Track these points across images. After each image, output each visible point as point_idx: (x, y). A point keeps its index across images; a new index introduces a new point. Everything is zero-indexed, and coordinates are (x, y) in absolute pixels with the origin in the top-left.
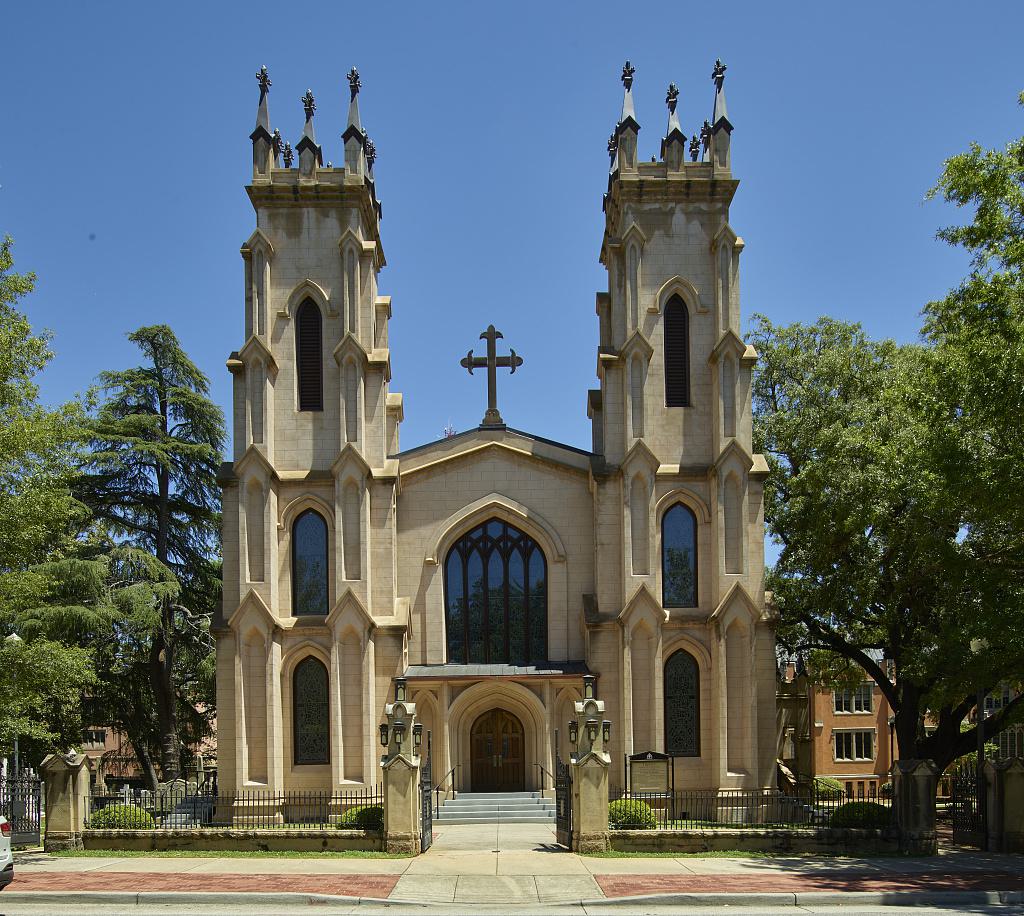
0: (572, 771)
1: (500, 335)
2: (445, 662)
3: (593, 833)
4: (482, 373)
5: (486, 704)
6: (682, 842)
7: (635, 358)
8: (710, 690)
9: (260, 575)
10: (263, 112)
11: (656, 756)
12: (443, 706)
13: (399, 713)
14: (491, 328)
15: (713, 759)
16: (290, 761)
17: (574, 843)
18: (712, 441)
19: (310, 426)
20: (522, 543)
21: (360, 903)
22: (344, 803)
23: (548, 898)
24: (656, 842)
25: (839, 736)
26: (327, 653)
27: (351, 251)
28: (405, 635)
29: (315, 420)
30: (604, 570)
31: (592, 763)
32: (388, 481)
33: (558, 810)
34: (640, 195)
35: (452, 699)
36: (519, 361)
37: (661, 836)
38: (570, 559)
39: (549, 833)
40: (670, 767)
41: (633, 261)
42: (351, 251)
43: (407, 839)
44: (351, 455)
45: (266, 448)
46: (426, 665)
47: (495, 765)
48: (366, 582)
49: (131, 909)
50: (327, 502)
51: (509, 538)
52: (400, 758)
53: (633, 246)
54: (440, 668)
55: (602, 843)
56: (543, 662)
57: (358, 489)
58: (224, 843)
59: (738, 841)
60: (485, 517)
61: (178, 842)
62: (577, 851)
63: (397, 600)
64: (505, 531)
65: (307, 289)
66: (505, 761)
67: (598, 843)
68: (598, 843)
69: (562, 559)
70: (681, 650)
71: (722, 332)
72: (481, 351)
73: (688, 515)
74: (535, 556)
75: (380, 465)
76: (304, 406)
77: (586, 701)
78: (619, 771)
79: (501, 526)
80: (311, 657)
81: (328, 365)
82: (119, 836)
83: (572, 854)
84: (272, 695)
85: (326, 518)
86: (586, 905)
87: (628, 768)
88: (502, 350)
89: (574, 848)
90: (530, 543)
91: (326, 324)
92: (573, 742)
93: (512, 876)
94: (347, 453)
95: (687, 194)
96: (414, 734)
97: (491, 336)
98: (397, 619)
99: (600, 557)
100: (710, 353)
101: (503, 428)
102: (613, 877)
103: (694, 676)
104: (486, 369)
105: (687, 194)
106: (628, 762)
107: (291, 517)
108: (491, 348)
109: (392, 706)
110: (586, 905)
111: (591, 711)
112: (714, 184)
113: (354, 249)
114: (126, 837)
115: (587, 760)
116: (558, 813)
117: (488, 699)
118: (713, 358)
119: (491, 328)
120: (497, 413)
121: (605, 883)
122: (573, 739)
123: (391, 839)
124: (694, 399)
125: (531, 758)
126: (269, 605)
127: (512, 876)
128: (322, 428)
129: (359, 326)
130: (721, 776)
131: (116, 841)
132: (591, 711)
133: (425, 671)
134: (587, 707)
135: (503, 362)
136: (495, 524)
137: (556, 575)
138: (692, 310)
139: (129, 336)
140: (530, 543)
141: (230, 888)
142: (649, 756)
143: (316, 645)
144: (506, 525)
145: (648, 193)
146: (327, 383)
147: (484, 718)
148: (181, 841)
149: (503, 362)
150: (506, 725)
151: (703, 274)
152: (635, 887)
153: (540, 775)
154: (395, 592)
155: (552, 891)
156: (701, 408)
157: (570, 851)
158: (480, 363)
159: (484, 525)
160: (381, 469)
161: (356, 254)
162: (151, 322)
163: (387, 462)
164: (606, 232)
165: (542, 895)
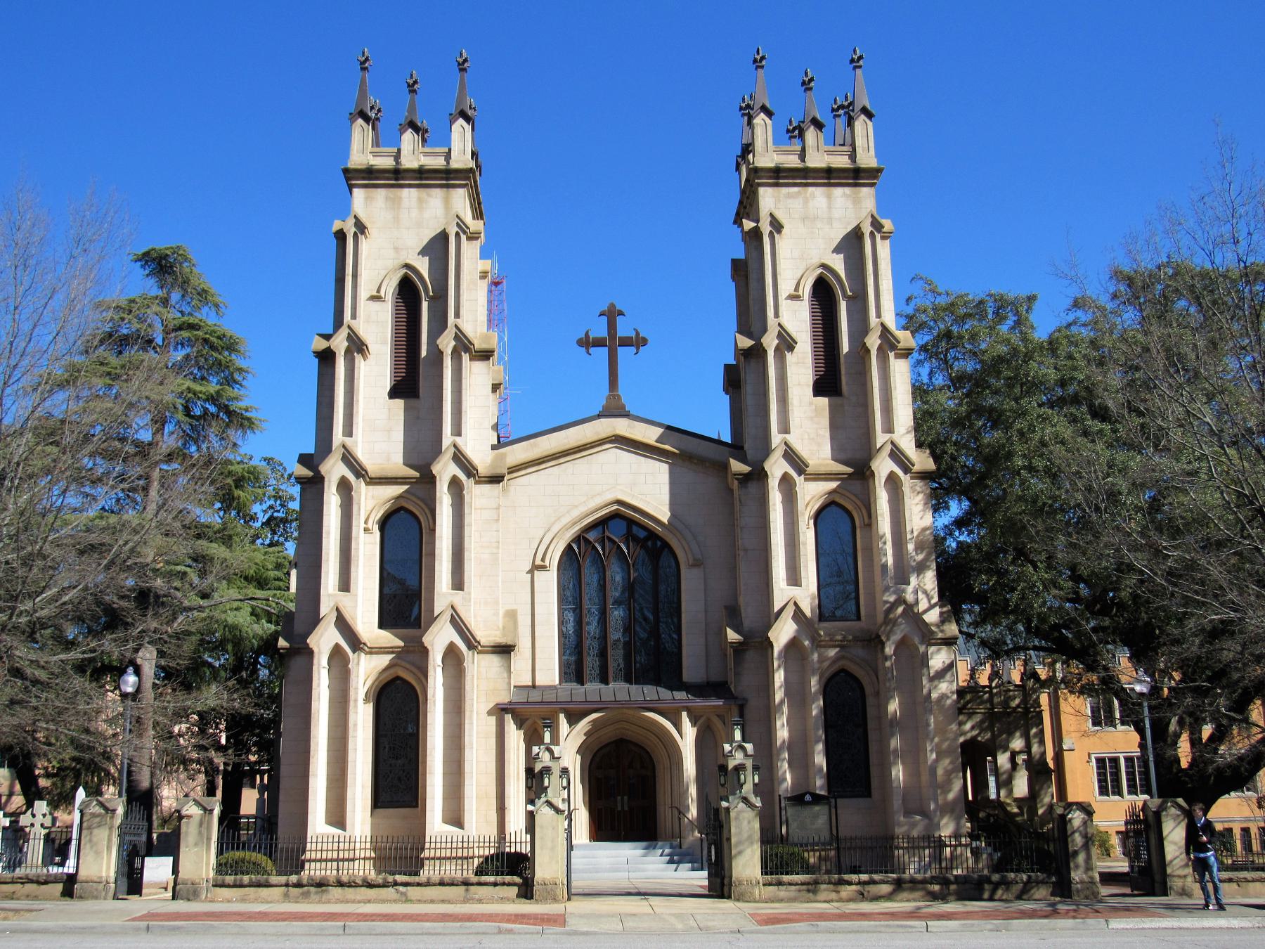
1: (621, 313)
4: (603, 352)
10: (363, 82)
11: (817, 799)
14: (612, 306)
17: (726, 889)
20: (650, 543)
23: (707, 928)
25: (1101, 762)
36: (644, 342)
40: (833, 810)
45: (356, 442)
47: (619, 808)
50: (422, 500)
56: (676, 683)
69: (697, 564)
72: (600, 329)
73: (845, 515)
74: (665, 559)
78: (774, 816)
79: (623, 524)
80: (398, 678)
84: (355, 725)
85: (420, 517)
88: (624, 330)
89: (726, 894)
90: (659, 543)
97: (612, 315)
104: (606, 349)
106: (783, 805)
108: (612, 326)
119: (612, 306)
121: (758, 918)
124: (845, 388)
128: (418, 418)
135: (626, 342)
136: (617, 521)
137: (690, 581)
139: (131, 257)
140: (659, 543)
142: (808, 798)
143: (408, 666)
149: (626, 342)
155: (710, 924)
158: (599, 343)
162: (161, 243)
164: (741, 202)
165: (701, 925)
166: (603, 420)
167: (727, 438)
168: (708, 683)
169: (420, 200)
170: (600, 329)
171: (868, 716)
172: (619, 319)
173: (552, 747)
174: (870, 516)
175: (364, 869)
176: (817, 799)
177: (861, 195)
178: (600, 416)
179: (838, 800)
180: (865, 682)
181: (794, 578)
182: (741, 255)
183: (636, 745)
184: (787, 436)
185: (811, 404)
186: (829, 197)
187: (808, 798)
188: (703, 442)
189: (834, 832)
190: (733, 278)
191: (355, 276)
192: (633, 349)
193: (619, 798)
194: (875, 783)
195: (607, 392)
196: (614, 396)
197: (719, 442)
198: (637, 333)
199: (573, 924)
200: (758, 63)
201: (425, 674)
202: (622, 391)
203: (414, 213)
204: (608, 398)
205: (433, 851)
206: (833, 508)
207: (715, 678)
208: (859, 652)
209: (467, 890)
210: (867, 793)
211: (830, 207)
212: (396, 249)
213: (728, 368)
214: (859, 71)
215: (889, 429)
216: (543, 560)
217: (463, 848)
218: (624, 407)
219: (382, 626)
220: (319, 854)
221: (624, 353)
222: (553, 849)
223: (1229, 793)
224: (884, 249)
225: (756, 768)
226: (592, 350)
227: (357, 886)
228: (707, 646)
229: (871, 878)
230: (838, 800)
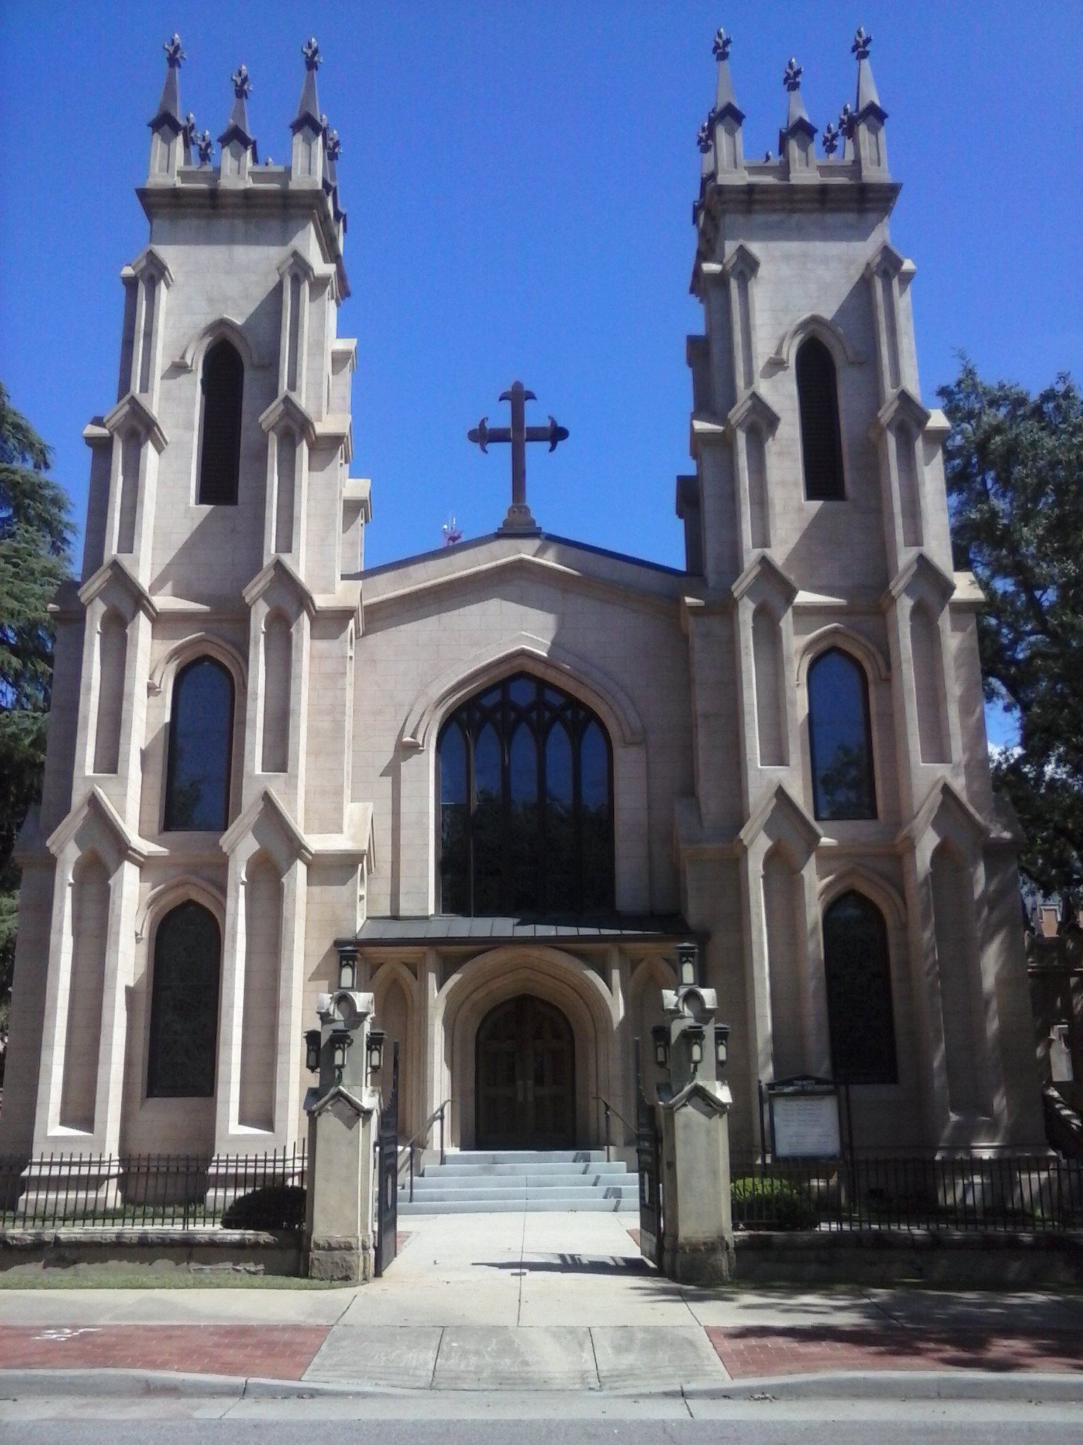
1: (530, 396)
5: (505, 987)
14: (518, 386)
20: (569, 714)
45: (137, 562)
52: (340, 1094)
64: (540, 693)
72: (501, 418)
75: (328, 590)
80: (191, 902)
88: (535, 417)
90: (582, 714)
96: (369, 1048)
97: (518, 397)
119: (518, 386)
122: (661, 1058)
124: (849, 488)
126: (122, 813)
135: (536, 435)
138: (839, 360)
140: (582, 714)
143: (204, 884)
149: (536, 435)
158: (498, 436)
163: (341, 585)
167: (681, 565)
170: (501, 418)
172: (528, 404)
174: (889, 666)
175: (112, 1195)
178: (500, 535)
181: (778, 756)
183: (543, 1002)
190: (690, 363)
191: (149, 335)
195: (509, 503)
200: (721, 52)
201: (223, 890)
202: (531, 500)
204: (511, 511)
206: (834, 659)
212: (211, 300)
213: (693, 341)
214: (865, 63)
215: (916, 538)
216: (413, 736)
217: (265, 1161)
218: (533, 522)
221: (535, 452)
222: (350, 1179)
224: (904, 302)
225: (721, 1036)
226: (490, 446)
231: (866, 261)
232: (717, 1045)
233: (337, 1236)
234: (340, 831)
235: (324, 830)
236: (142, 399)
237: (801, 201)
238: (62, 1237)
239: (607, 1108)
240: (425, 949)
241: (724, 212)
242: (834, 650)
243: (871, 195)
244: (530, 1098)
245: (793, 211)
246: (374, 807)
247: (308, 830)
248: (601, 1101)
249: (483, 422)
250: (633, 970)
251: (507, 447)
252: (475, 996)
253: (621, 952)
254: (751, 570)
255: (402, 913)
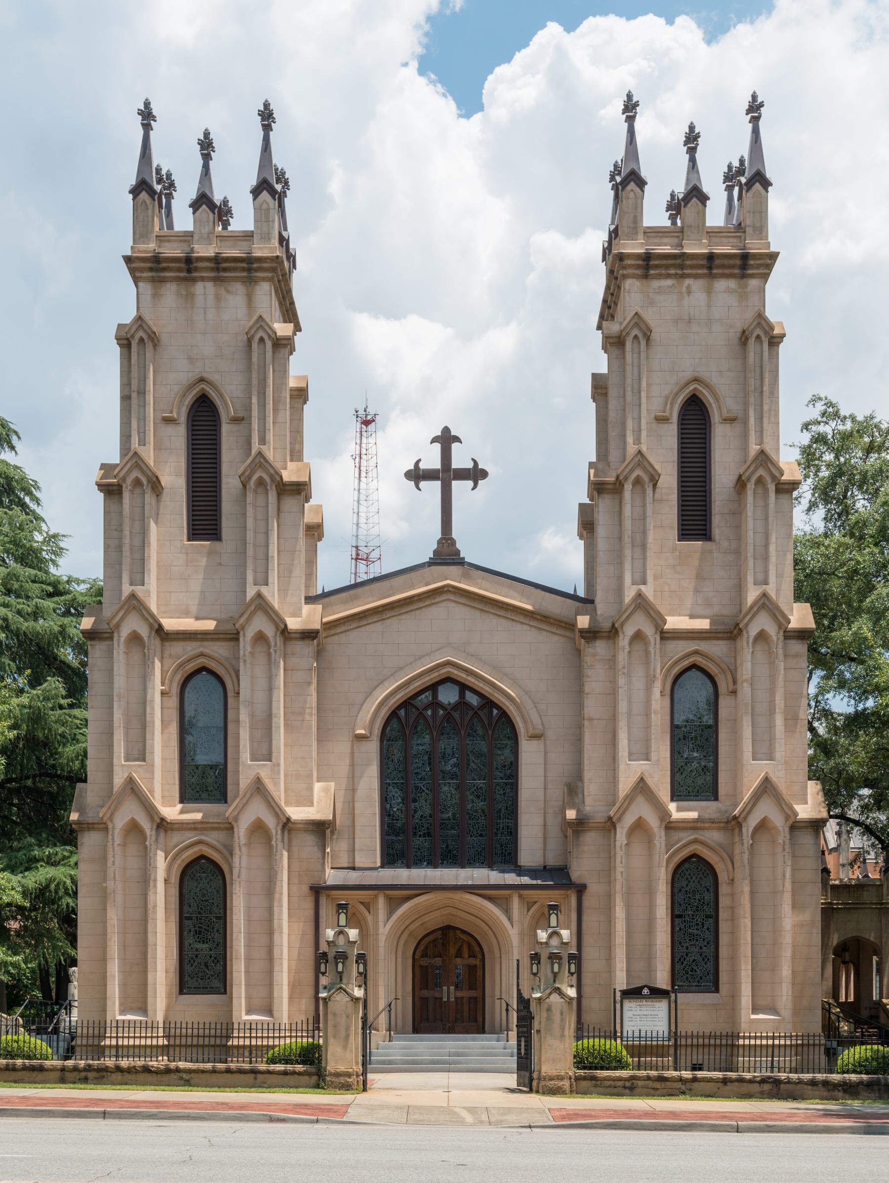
0: (533, 1007)
2: (379, 864)
3: (555, 1073)
5: (435, 920)
6: (657, 1085)
7: (638, 482)
8: (732, 908)
9: (140, 753)
12: (377, 922)
13: (341, 940)
15: (735, 996)
16: (175, 989)
17: (535, 1083)
18: (740, 588)
19: (204, 561)
21: (317, 1121)
22: (265, 1043)
24: (628, 1084)
26: (228, 856)
27: (262, 340)
28: (328, 832)
29: (210, 553)
30: (592, 753)
31: (555, 998)
32: (308, 635)
33: (519, 1049)
34: (647, 267)
35: (390, 913)
37: (633, 1078)
38: (550, 734)
39: (511, 1080)
40: (673, 1005)
41: (636, 356)
42: (262, 340)
43: (349, 1075)
44: (261, 604)
45: (148, 592)
46: (354, 869)
48: (279, 765)
49: (100, 1122)
51: (469, 706)
52: (341, 988)
53: (636, 337)
54: (374, 874)
55: (566, 1084)
57: (269, 648)
58: (142, 1077)
59: (720, 1085)
60: (434, 676)
61: (90, 1075)
62: (537, 1092)
63: (318, 786)
64: (462, 695)
65: (203, 386)
66: (459, 994)
67: (561, 1083)
68: (561, 1083)
70: (694, 855)
71: (754, 448)
72: (432, 460)
75: (297, 614)
76: (195, 533)
77: (550, 930)
80: (203, 857)
81: (230, 483)
82: (25, 1068)
83: (533, 1095)
86: (534, 1127)
87: (618, 1006)
88: (460, 459)
89: (534, 1088)
91: (228, 434)
92: (535, 974)
93: (464, 1108)
94: (256, 602)
95: (710, 268)
96: (357, 962)
97: (446, 440)
98: (318, 812)
99: (586, 730)
100: (736, 477)
101: (461, 562)
102: (568, 1110)
103: (711, 889)
105: (710, 268)
107: (179, 678)
109: (333, 933)
110: (534, 1127)
111: (555, 942)
112: (745, 257)
113: (266, 337)
114: (33, 1069)
115: (550, 994)
116: (519, 1053)
117: (437, 914)
118: (741, 484)
119: (446, 430)
120: (453, 542)
122: (535, 971)
123: (331, 1074)
125: (493, 991)
126: (152, 792)
127: (464, 1108)
129: (270, 437)
130: (743, 1019)
131: (20, 1073)
132: (555, 942)
133: (353, 878)
134: (550, 936)
135: (462, 474)
138: (715, 417)
140: (495, 712)
141: (186, 1108)
142: (646, 991)
144: (463, 687)
145: (657, 267)
146: (227, 506)
147: (431, 937)
148: (94, 1074)
149: (462, 474)
150: (461, 947)
151: (729, 370)
152: (584, 1116)
153: (504, 1013)
154: (315, 774)
156: (725, 544)
157: (531, 1091)
158: (430, 475)
159: (433, 688)
160: (300, 619)
161: (269, 344)
163: (306, 609)
166: (433, 568)
168: (545, 867)
169: (218, 297)
171: (720, 906)
172: (455, 446)
173: (346, 930)
176: (657, 993)
177: (749, 289)
179: (679, 995)
180: (720, 868)
182: (603, 368)
183: (464, 932)
184: (642, 587)
185: (674, 549)
186: (709, 291)
187: (646, 991)
188: (547, 594)
189: (673, 1029)
190: (594, 398)
192: (470, 483)
193: (445, 988)
194: (723, 977)
196: (447, 540)
197: (574, 597)
198: (475, 463)
199: (352, 1114)
203: (211, 313)
204: (440, 542)
205: (207, 1039)
206: (694, 673)
207: (552, 861)
208: (715, 836)
209: (255, 1078)
210: (715, 988)
211: (709, 306)
212: (191, 360)
218: (458, 552)
219: (183, 799)
220: (189, 1040)
223: (486, 79)
227: (137, 1072)
228: (545, 825)
229: (213, 1067)
230: (679, 995)
231: (740, 330)
232: (570, 964)
233: (342, 1068)
234: (312, 805)
235: (299, 804)
236: (142, 451)
237: (692, 267)
238: (181, 1066)
239: (507, 1005)
240: (376, 892)
241: (625, 277)
242: (694, 666)
243: (752, 262)
244: (452, 999)
245: (683, 276)
246: (335, 785)
247: (287, 803)
248: (503, 1001)
249: (417, 463)
250: (528, 911)
251: (437, 484)
252: (412, 927)
253: (520, 896)
254: (630, 605)
255: (357, 865)
